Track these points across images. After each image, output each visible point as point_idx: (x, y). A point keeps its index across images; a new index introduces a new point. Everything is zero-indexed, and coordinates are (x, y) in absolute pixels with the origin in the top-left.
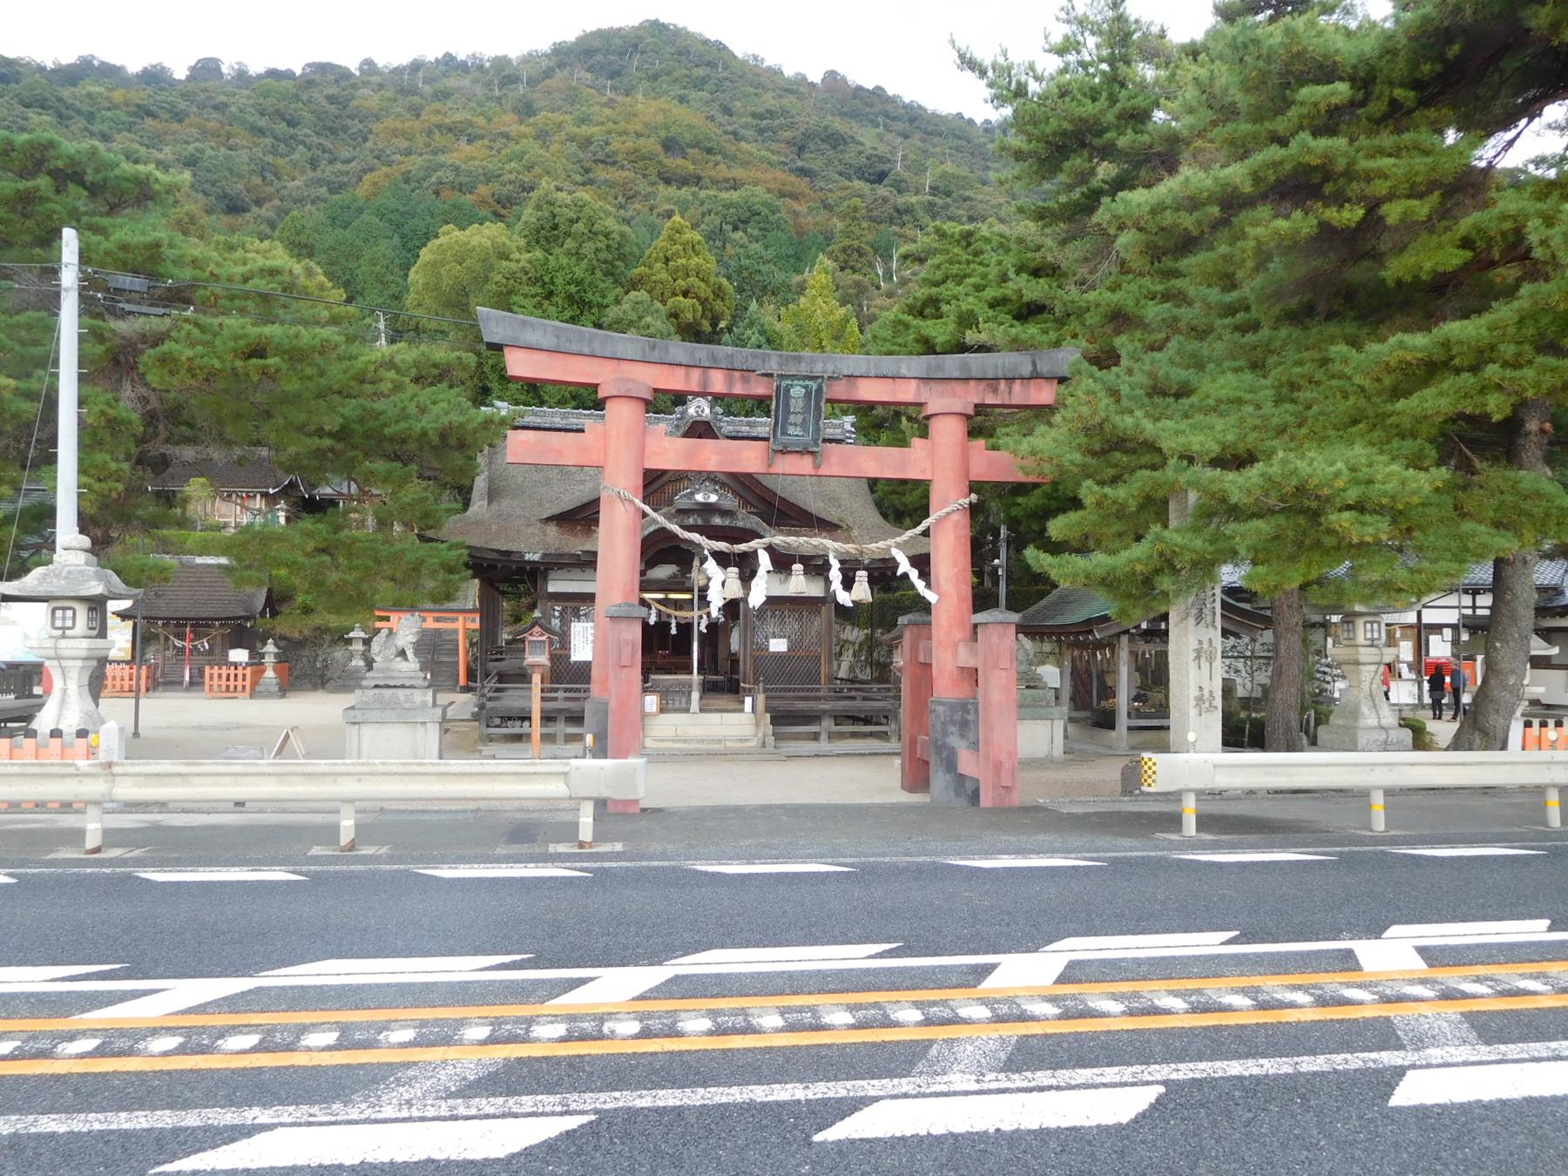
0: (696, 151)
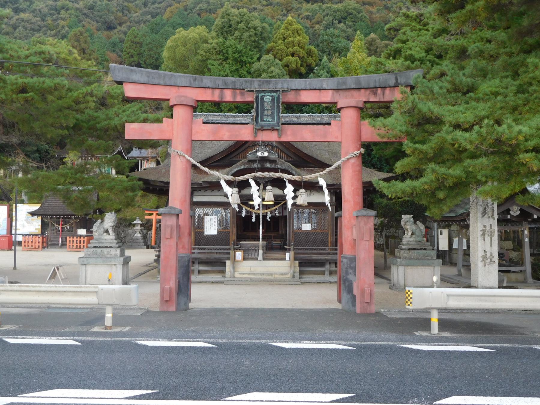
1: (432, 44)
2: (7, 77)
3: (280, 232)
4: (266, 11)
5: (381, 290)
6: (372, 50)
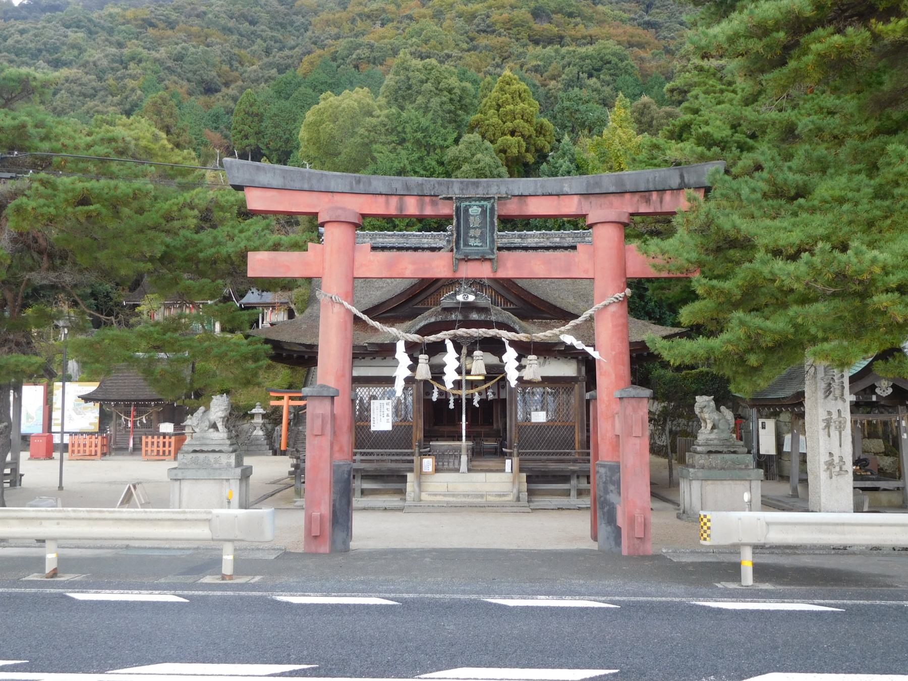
0: (560, 15)
1: (741, 118)
2: (59, 180)
3: (495, 426)
4: (468, 59)
5: (662, 520)
6: (644, 124)
